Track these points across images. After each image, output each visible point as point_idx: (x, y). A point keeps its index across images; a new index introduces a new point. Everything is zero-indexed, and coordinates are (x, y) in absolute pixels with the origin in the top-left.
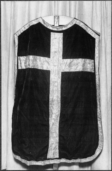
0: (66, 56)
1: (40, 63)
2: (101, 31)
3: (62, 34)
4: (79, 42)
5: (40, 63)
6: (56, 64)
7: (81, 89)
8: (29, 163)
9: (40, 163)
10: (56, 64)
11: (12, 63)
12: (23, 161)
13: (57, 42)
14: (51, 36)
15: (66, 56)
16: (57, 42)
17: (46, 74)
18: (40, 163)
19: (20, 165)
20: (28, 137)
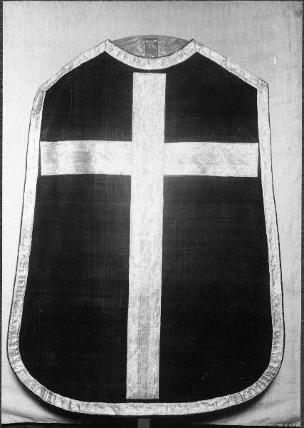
0: (173, 134)
1: (105, 158)
2: (115, 411)
3: (164, 76)
4: (208, 101)
5: (105, 158)
6: (147, 161)
7: (220, 224)
8: (59, 401)
9: (107, 409)
10: (147, 161)
11: (32, 158)
12: (47, 396)
13: (149, 98)
14: (135, 82)
15: (173, 134)
16: (149, 98)
17: (119, 187)
18: (107, 409)
19: (248, 413)
20: (69, 325)
